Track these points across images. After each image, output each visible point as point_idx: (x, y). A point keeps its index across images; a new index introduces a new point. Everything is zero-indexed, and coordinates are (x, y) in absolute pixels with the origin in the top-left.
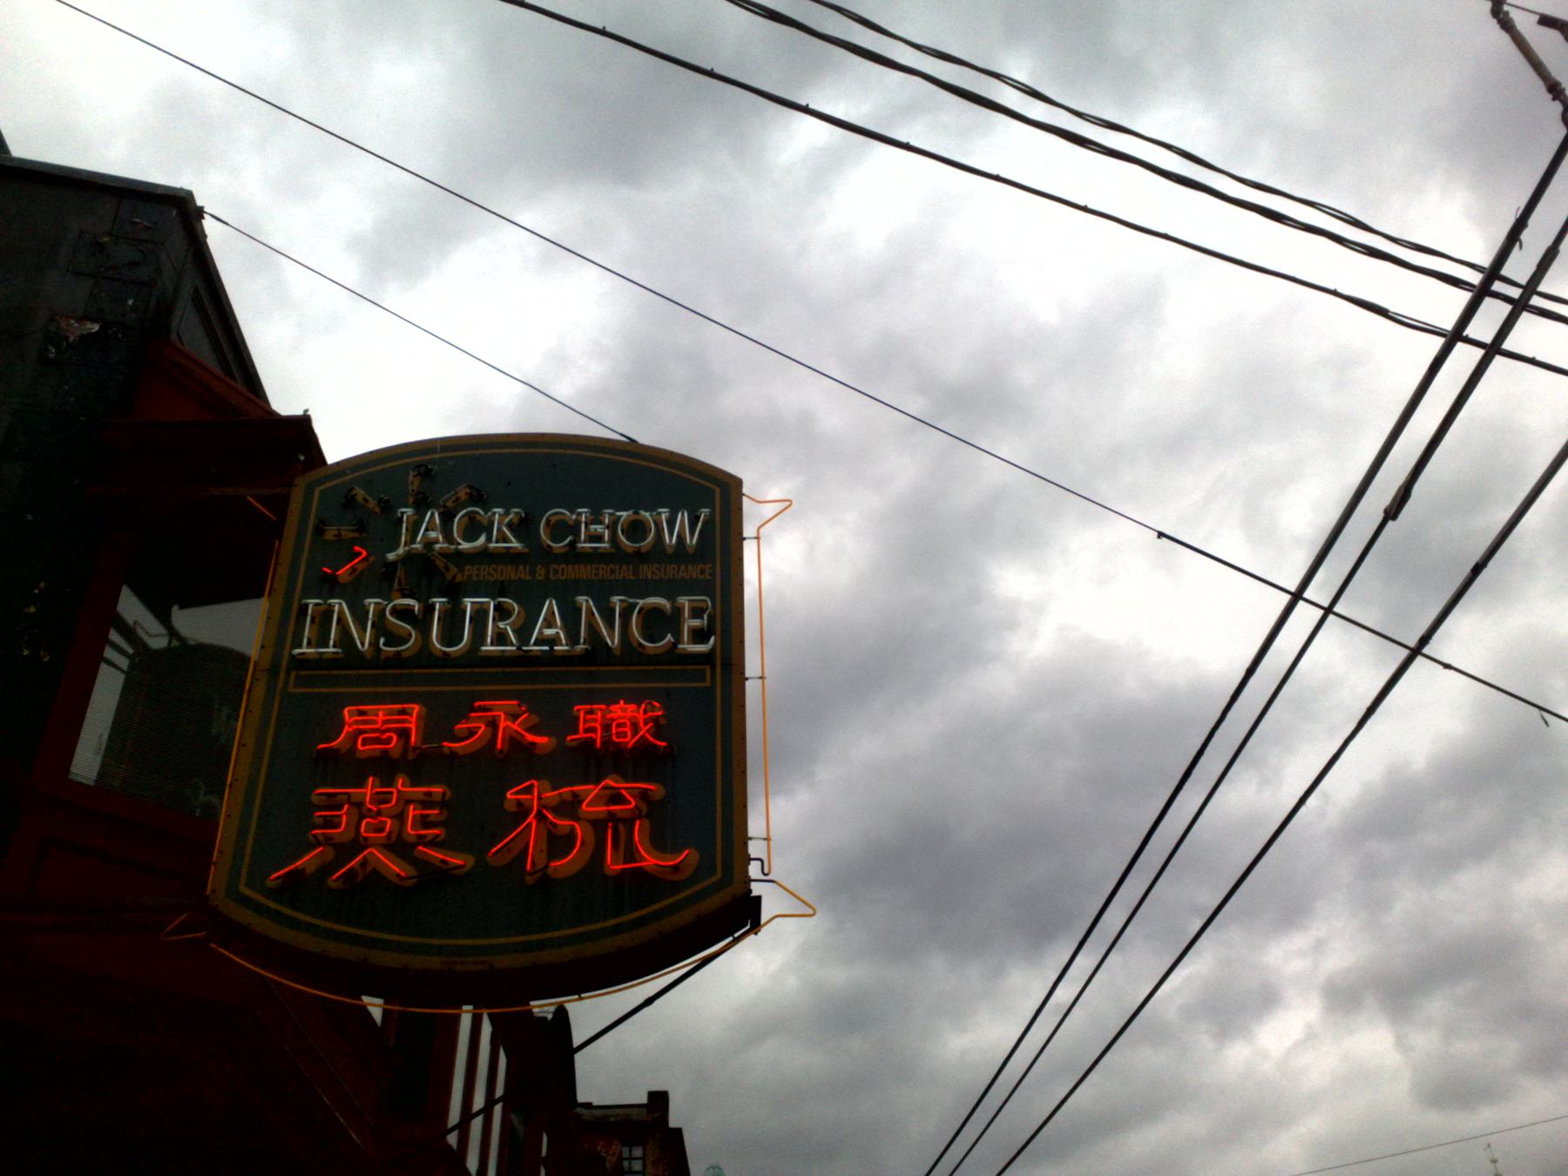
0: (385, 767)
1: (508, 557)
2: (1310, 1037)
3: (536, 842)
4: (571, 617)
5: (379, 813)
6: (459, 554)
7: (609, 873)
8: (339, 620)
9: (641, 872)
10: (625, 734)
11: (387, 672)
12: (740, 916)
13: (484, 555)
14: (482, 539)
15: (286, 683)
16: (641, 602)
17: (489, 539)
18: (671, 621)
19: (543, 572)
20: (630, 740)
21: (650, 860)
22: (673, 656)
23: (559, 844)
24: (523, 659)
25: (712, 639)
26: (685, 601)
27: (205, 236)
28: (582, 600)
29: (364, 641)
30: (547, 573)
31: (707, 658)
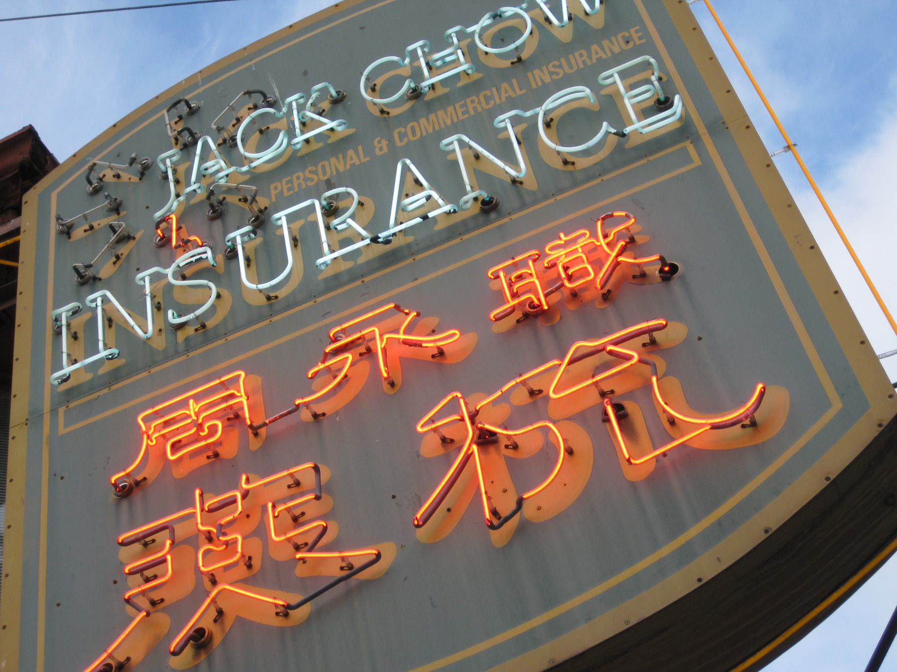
0: (215, 465)
1: (333, 146)
2: (331, 96)
3: (489, 482)
4: (445, 177)
5: (223, 530)
6: (255, 177)
7: (631, 475)
8: (109, 322)
9: (689, 456)
10: (585, 273)
11: (196, 343)
12: (830, 405)
13: (291, 163)
14: (282, 139)
15: (54, 425)
16: (541, 111)
17: (291, 134)
18: (610, 106)
19: (384, 143)
20: (595, 277)
21: (697, 427)
22: (627, 152)
23: (525, 467)
24: (391, 256)
25: (677, 98)
26: (612, 77)
27: (180, 84)
28: (452, 143)
29: (146, 328)
30: (391, 141)
31: (685, 130)
